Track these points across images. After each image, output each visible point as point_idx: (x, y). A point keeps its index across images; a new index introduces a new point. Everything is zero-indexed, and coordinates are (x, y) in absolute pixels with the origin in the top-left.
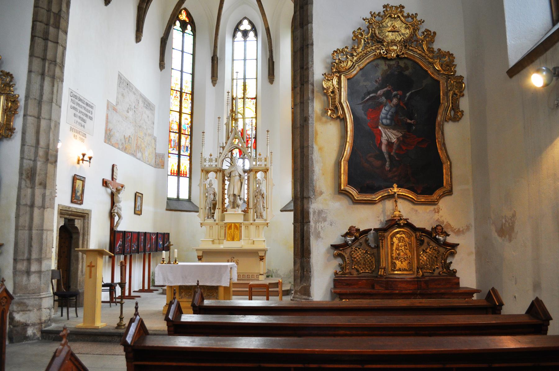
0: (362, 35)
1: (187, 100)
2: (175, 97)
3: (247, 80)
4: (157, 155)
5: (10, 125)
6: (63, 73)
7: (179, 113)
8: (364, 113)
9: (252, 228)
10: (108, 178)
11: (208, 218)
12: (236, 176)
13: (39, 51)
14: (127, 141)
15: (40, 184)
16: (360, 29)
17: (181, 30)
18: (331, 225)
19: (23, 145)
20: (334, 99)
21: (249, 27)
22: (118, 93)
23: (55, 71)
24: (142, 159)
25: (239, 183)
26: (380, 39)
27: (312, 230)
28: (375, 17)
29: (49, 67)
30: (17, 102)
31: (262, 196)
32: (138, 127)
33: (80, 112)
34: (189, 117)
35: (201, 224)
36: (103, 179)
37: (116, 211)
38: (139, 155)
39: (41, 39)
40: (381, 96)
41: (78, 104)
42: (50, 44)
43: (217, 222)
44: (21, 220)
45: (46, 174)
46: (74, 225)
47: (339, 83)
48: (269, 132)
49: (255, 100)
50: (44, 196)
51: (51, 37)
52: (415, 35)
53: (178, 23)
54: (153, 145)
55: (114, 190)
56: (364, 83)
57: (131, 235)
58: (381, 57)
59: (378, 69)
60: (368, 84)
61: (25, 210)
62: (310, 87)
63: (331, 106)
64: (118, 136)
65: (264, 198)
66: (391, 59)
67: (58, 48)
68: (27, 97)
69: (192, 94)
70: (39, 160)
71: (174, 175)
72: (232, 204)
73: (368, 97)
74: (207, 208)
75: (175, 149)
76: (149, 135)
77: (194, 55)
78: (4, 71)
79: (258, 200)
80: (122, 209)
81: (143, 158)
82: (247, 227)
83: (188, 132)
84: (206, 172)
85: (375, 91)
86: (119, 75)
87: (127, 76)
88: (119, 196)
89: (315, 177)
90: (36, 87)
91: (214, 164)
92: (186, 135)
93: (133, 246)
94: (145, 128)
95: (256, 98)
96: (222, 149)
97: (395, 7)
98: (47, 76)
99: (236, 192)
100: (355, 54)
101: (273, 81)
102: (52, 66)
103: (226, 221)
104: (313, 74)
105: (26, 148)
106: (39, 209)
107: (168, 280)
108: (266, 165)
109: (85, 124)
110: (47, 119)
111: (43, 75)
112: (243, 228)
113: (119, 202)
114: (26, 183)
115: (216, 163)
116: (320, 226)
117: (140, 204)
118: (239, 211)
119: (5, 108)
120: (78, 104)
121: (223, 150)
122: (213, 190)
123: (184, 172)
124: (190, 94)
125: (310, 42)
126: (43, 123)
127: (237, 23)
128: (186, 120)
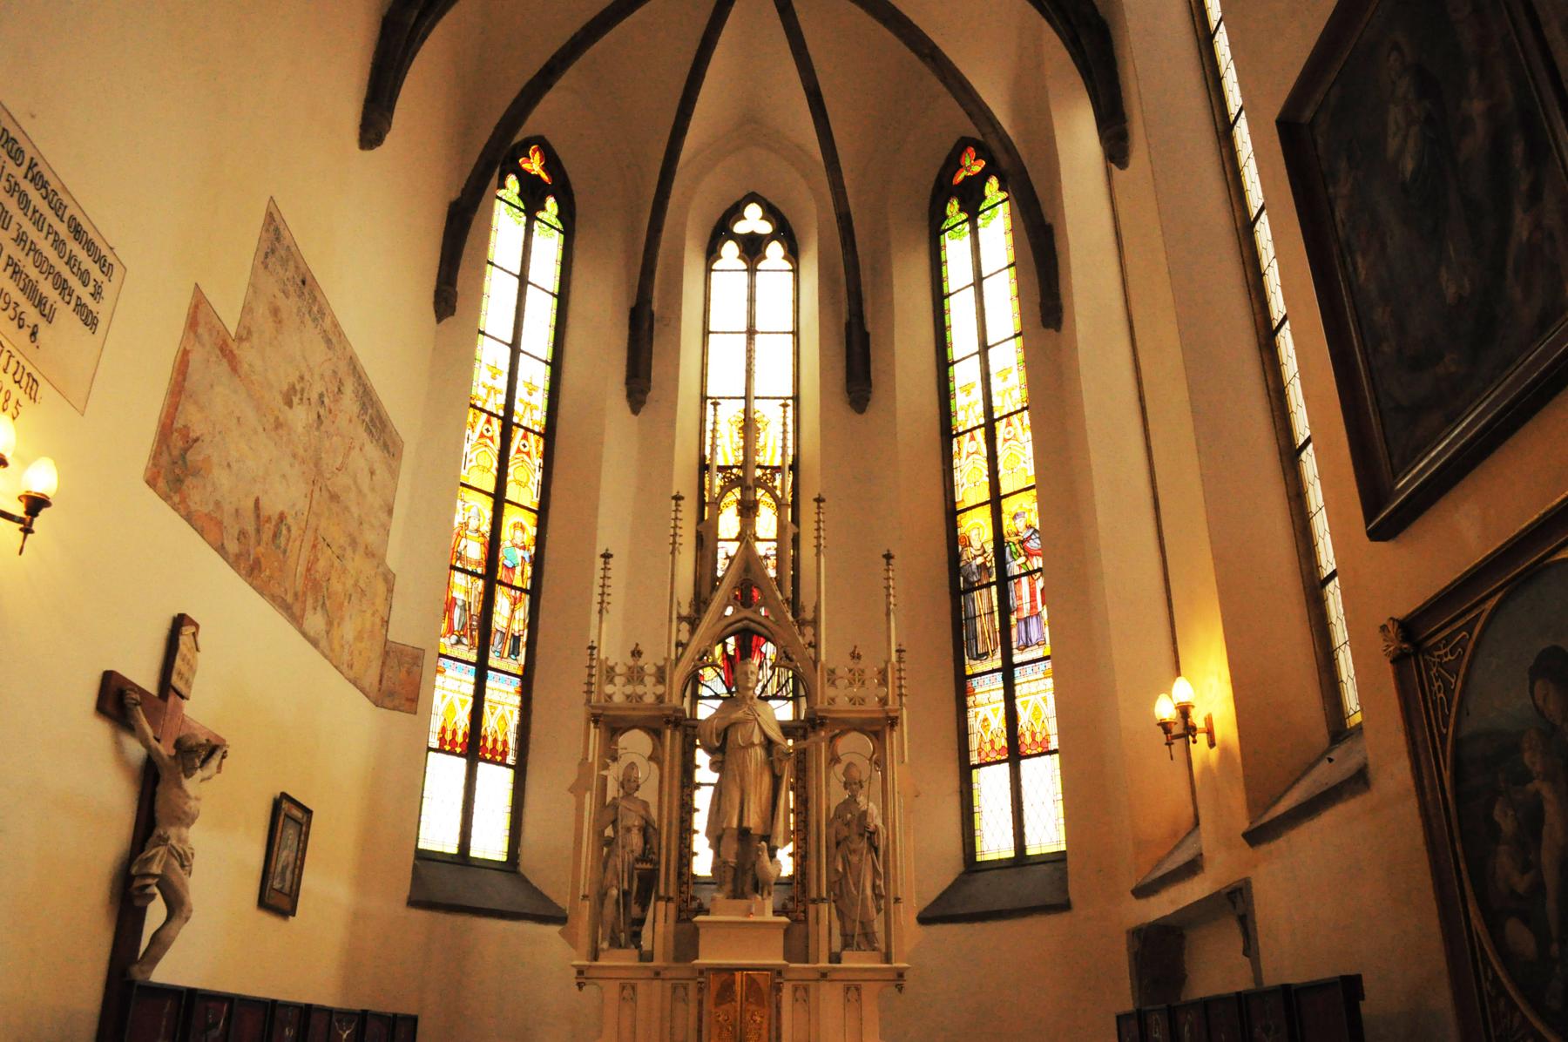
1: (528, 454)
2: (482, 436)
3: (757, 405)
7: (491, 500)
9: (830, 998)
11: (615, 943)
12: (753, 745)
14: (267, 535)
17: (522, 207)
21: (765, 228)
24: (323, 643)
25: (767, 780)
31: (871, 836)
32: (325, 495)
34: (530, 520)
36: (109, 677)
37: (156, 869)
43: (657, 963)
48: (892, 561)
53: (512, 182)
54: (379, 601)
55: (165, 750)
57: (228, 1020)
71: (452, 753)
72: (729, 875)
75: (465, 640)
76: (370, 554)
79: (854, 859)
80: (197, 864)
81: (330, 643)
82: (803, 990)
83: (523, 577)
84: (611, 724)
88: (191, 785)
91: (649, 691)
94: (356, 515)
96: (685, 626)
99: (754, 821)
101: (868, 400)
103: (704, 960)
108: (883, 701)
109: (42, 324)
113: (186, 819)
115: (660, 689)
117: (291, 859)
118: (765, 909)
121: (692, 631)
122: (643, 813)
123: (495, 741)
124: (539, 434)
128: (519, 530)
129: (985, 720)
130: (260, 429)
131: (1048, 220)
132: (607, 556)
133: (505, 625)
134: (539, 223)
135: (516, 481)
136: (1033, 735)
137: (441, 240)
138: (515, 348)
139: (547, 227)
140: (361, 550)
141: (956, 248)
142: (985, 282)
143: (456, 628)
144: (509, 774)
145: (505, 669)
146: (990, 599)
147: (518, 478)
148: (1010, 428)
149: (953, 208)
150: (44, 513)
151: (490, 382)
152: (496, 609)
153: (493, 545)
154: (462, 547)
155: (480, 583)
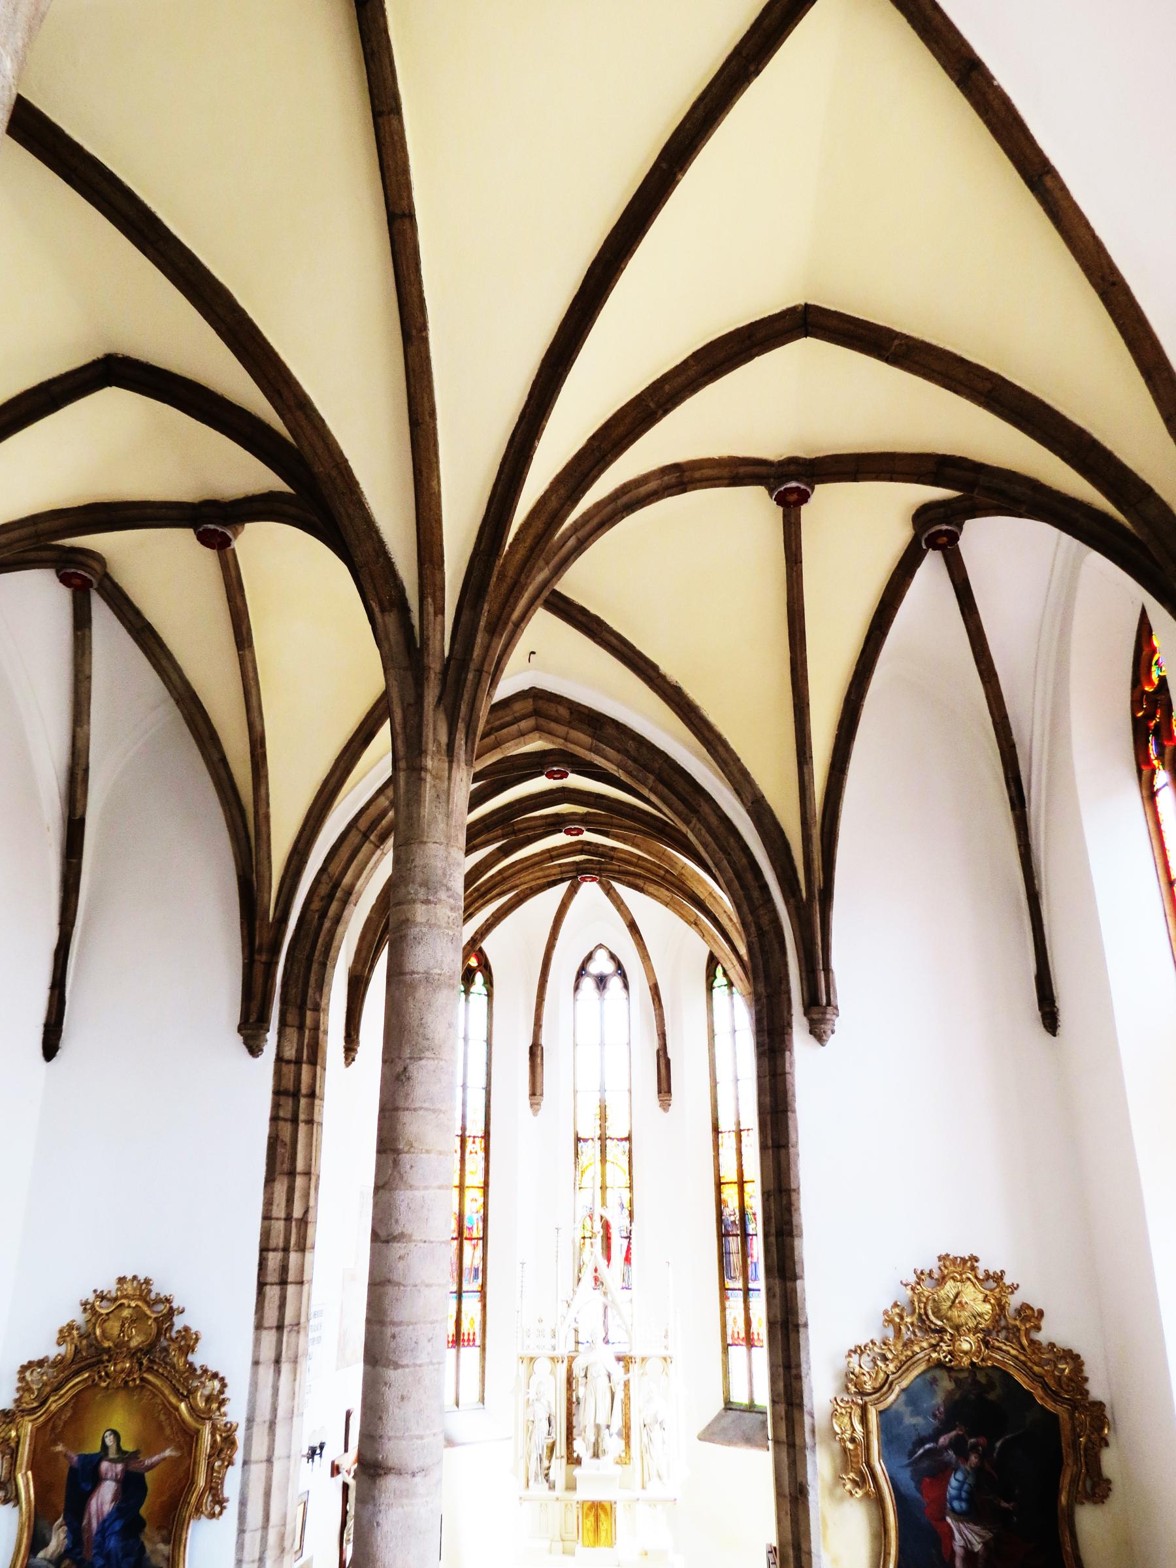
0: (902, 1318)
8: (915, 1487)
21: (609, 968)
35: (521, 1498)
40: (946, 1448)
49: (626, 1144)
52: (1002, 1317)
56: (911, 1419)
59: (935, 1387)
60: (919, 1420)
62: (807, 1419)
66: (962, 1370)
68: (250, 1421)
73: (921, 1451)
85: (934, 1437)
95: (629, 1139)
97: (961, 1258)
99: (602, 1421)
123: (469, 1334)
137: (259, 492)
140: (546, 1472)
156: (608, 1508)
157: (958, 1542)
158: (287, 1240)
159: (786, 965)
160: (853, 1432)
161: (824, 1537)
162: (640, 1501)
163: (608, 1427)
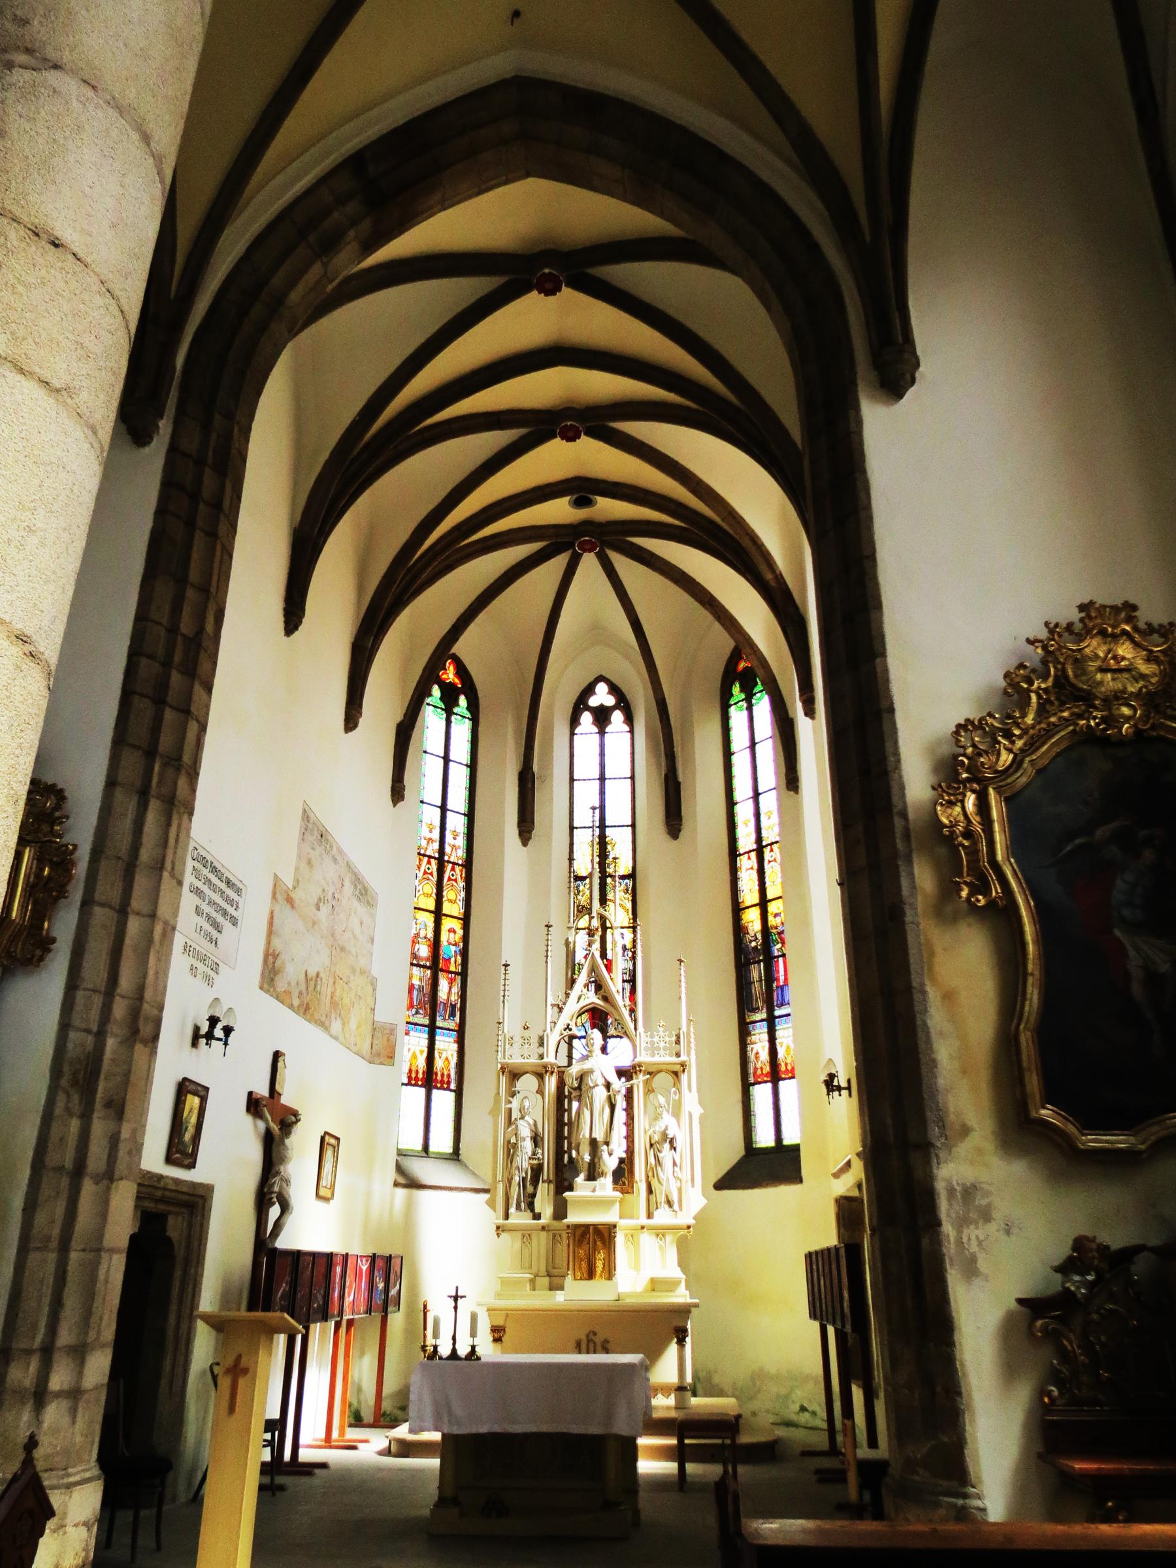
1: (455, 880)
2: (425, 873)
3: (608, 831)
4: (375, 1029)
5: (42, 928)
6: (194, 791)
10: (263, 1090)
13: (139, 731)
15: (109, 1104)
16: (1021, 666)
17: (444, 707)
18: (1008, 1232)
19: (72, 987)
20: (973, 852)
21: (610, 701)
22: (299, 856)
23: (175, 783)
24: (342, 1039)
25: (607, 1111)
26: (1081, 690)
27: (950, 1249)
28: (1060, 635)
29: (161, 775)
30: (69, 866)
32: (338, 949)
33: (211, 903)
34: (457, 925)
36: (250, 1094)
38: (336, 1026)
39: (146, 700)
41: (208, 881)
42: (169, 715)
44: (40, 1218)
45: (127, 1074)
46: (165, 1230)
47: (983, 807)
49: (629, 882)
50: (114, 1141)
51: (171, 698)
53: (436, 691)
58: (1090, 738)
61: (55, 1187)
62: (898, 823)
63: (968, 875)
64: (291, 974)
65: (675, 1149)
67: (189, 726)
68: (97, 852)
69: (468, 864)
70: (112, 1033)
71: (416, 1085)
73: (1069, 848)
74: (516, 1179)
75: (421, 1011)
76: (363, 972)
77: (473, 766)
78: (40, 780)
86: (305, 811)
87: (324, 816)
89: (941, 1082)
90: (125, 825)
92: (452, 972)
93: (316, 1294)
95: (632, 876)
97: (1111, 607)
98: (154, 796)
99: (599, 1135)
100: (1017, 732)
101: (680, 831)
102: (170, 771)
104: (902, 788)
105: (80, 995)
106: (97, 1184)
107: (450, 1413)
110: (144, 916)
111: (144, 794)
112: (620, 1240)
114: (68, 1102)
116: (973, 1238)
119: (31, 880)
120: (208, 881)
123: (443, 1075)
124: (462, 865)
125: (884, 704)
126: (134, 926)
127: (580, 692)
129: (757, 1053)
130: (306, 932)
131: (791, 715)
132: (506, 965)
133: (446, 998)
134: (440, 1030)
135: (448, 900)
136: (786, 1065)
138: (444, 808)
139: (460, 718)
141: (738, 717)
142: (757, 746)
143: (415, 1004)
144: (452, 1095)
145: (447, 1027)
146: (760, 970)
147: (450, 898)
148: (772, 853)
149: (736, 689)
150: (232, 1034)
151: (428, 835)
152: (440, 988)
153: (436, 945)
154: (416, 950)
155: (429, 972)
156: (606, 1235)
157: (1134, 963)
158: (170, 655)
159: (845, 322)
160: (968, 825)
161: (931, 969)
162: (645, 1230)
163: (607, 1143)
